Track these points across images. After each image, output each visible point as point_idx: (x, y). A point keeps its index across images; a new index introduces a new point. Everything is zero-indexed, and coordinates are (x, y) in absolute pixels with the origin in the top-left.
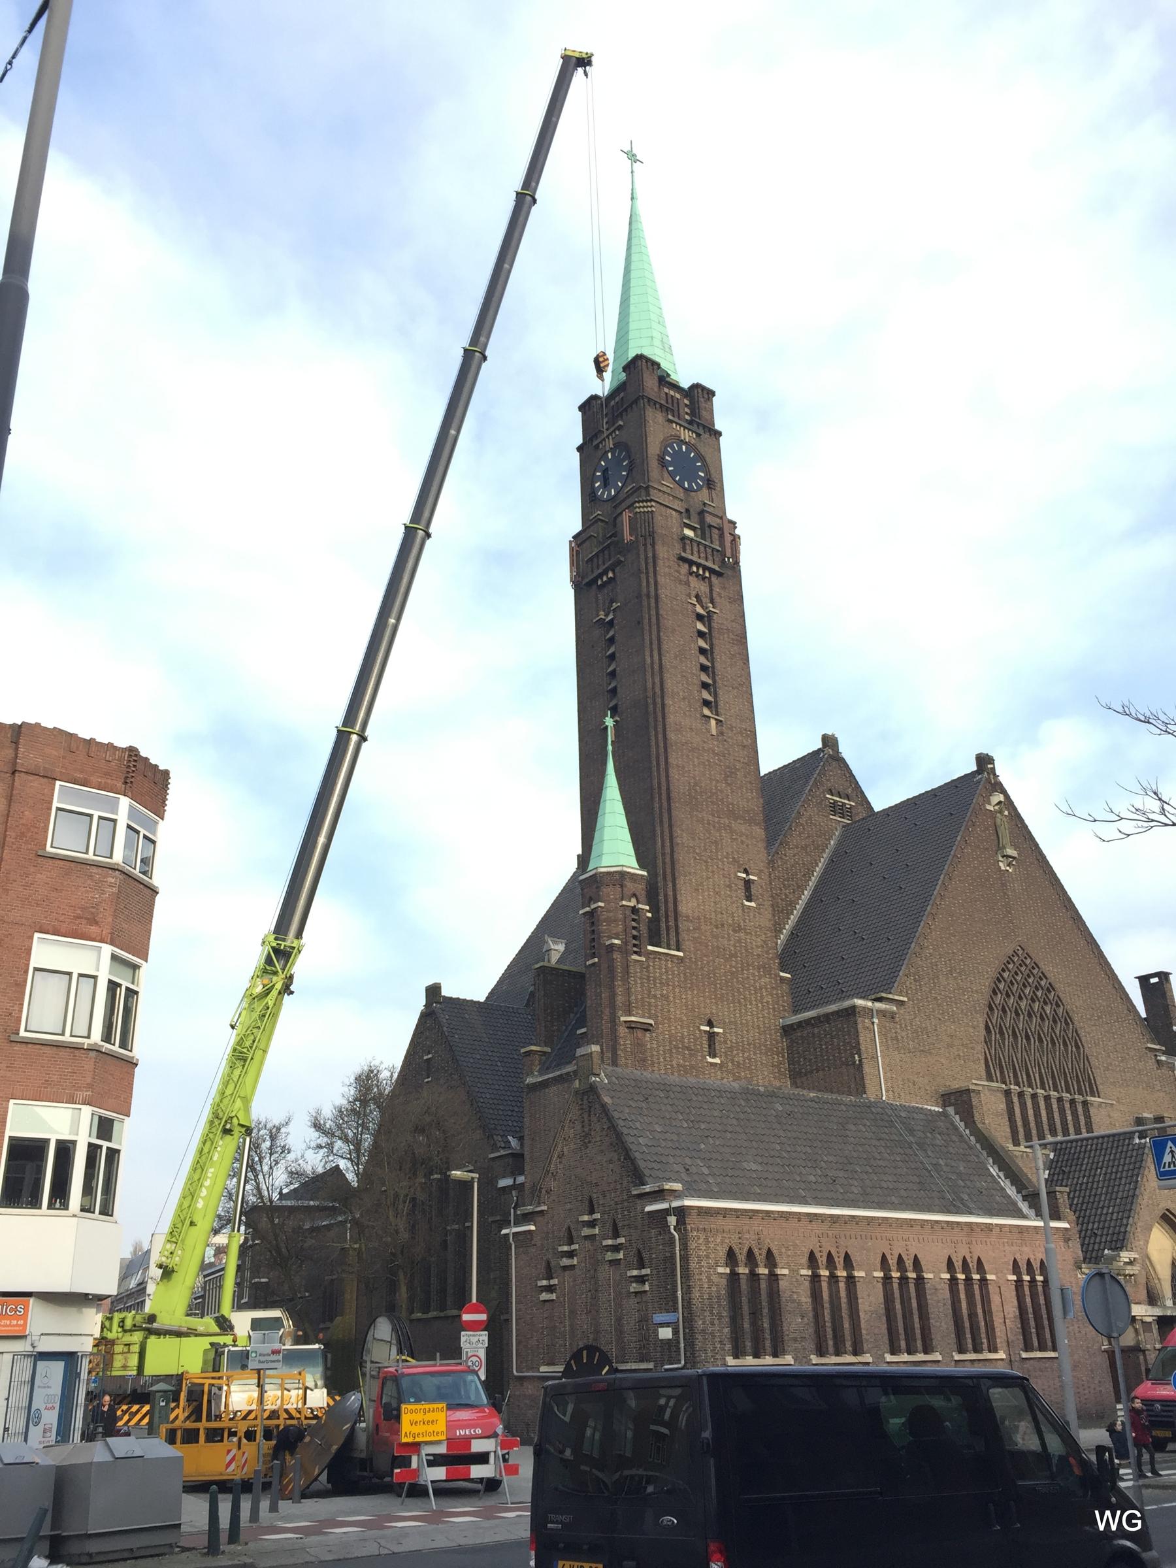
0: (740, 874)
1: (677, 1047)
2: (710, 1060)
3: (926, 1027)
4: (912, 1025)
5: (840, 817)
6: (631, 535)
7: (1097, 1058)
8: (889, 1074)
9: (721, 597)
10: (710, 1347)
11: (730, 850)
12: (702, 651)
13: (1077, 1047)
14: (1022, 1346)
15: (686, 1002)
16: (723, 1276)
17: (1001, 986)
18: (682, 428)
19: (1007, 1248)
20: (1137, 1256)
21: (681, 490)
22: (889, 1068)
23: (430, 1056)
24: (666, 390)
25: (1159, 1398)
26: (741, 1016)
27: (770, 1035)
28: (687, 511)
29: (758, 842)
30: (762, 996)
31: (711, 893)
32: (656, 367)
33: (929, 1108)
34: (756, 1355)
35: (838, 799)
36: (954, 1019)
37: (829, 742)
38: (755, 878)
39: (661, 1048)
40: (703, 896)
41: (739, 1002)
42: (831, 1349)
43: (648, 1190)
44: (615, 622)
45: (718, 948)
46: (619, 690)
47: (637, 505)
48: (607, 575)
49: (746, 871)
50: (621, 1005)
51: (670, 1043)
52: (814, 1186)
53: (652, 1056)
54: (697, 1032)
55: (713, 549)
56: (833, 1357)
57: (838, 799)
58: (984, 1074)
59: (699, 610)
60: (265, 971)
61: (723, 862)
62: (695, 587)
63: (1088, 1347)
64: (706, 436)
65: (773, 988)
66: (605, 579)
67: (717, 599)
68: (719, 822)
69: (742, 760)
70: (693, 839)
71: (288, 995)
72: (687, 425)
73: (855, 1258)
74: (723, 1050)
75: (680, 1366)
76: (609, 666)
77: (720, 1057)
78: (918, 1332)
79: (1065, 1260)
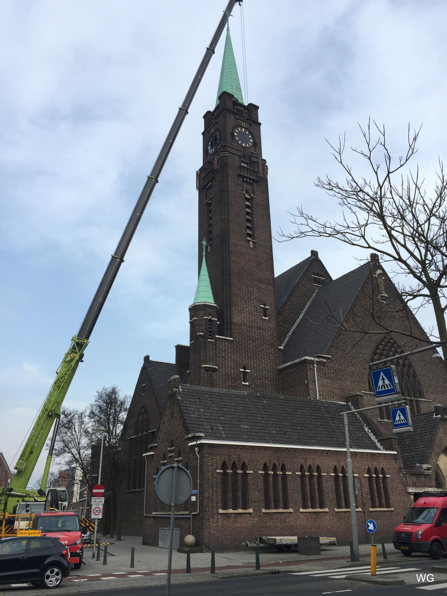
0: (261, 306)
1: (228, 378)
2: (243, 383)
3: (340, 369)
4: (333, 367)
5: (318, 284)
6: (218, 166)
7: (424, 382)
8: (321, 388)
9: (257, 191)
10: (211, 505)
11: (257, 296)
12: (248, 213)
13: (414, 377)
14: (370, 505)
15: (234, 359)
16: (220, 474)
17: (378, 351)
18: (243, 122)
19: (365, 462)
20: (431, 466)
21: (242, 147)
22: (321, 385)
23: (144, 385)
24: (237, 107)
25: (404, 531)
26: (259, 365)
27: (273, 373)
28: (244, 156)
29: (270, 292)
30: (270, 357)
31: (248, 314)
32: (231, 97)
33: (340, 403)
34: (313, 508)
35: (317, 277)
36: (354, 365)
37: (314, 253)
38: (269, 307)
39: (221, 378)
40: (244, 315)
41: (259, 359)
42: (273, 506)
43: (190, 436)
44: (212, 203)
45: (250, 336)
46: (212, 231)
47: (220, 153)
48: (209, 184)
49: (264, 305)
50: (202, 360)
51: (225, 376)
52: (274, 435)
53: (216, 382)
54: (238, 371)
55: (254, 171)
56: (273, 510)
57: (317, 277)
58: (368, 388)
59: (247, 196)
60: (72, 352)
61: (253, 301)
62: (246, 187)
63: (404, 506)
64: (254, 125)
65: (275, 353)
66: (209, 185)
67: (256, 192)
68: (252, 284)
69: (264, 258)
70: (240, 291)
71: (81, 362)
72: (246, 121)
73: (287, 466)
74: (250, 379)
75: (197, 513)
76: (210, 221)
77: (249, 382)
78: (317, 499)
79: (394, 468)
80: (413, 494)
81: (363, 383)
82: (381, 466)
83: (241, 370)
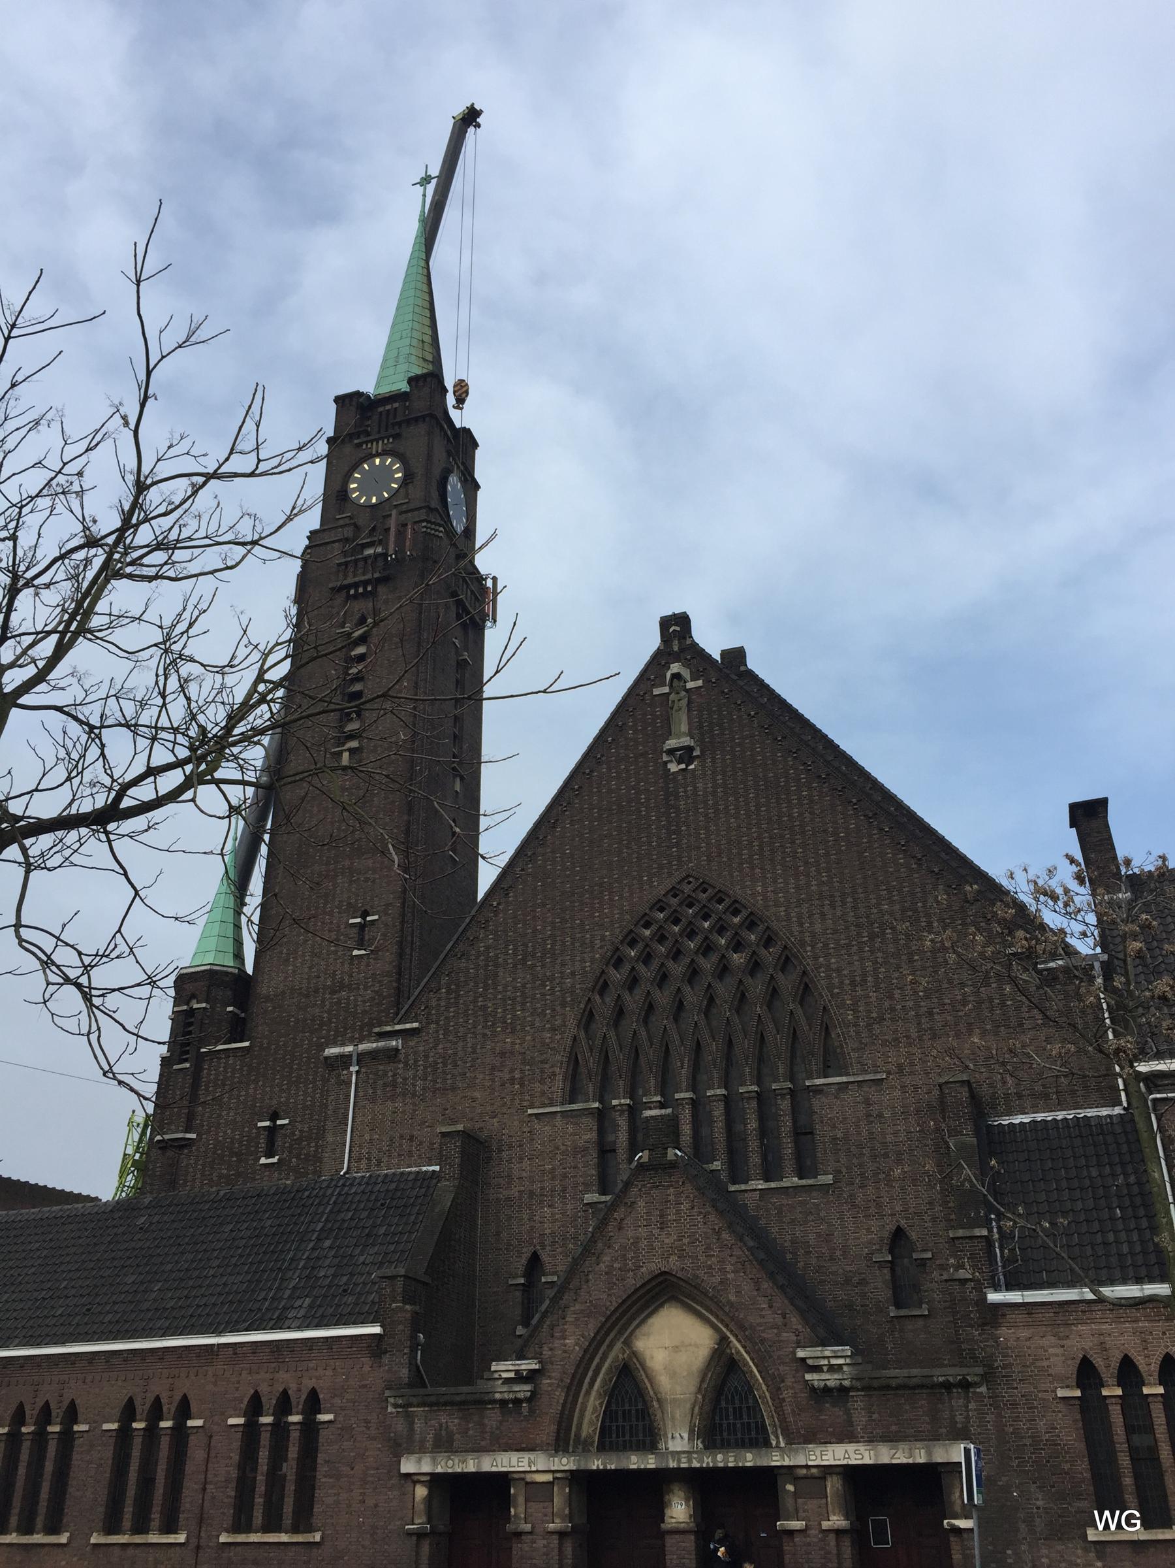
0: (351, 921)
14: (228, 1522)
54: (254, 1131)
79: (364, 1386)
80: (427, 1478)
81: (542, 1081)
82: (309, 1384)
83: (260, 1124)
